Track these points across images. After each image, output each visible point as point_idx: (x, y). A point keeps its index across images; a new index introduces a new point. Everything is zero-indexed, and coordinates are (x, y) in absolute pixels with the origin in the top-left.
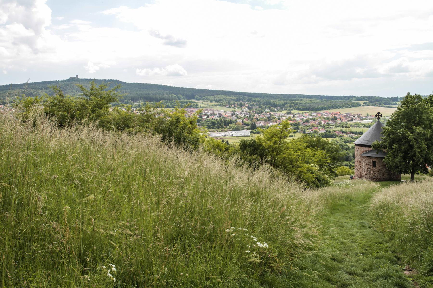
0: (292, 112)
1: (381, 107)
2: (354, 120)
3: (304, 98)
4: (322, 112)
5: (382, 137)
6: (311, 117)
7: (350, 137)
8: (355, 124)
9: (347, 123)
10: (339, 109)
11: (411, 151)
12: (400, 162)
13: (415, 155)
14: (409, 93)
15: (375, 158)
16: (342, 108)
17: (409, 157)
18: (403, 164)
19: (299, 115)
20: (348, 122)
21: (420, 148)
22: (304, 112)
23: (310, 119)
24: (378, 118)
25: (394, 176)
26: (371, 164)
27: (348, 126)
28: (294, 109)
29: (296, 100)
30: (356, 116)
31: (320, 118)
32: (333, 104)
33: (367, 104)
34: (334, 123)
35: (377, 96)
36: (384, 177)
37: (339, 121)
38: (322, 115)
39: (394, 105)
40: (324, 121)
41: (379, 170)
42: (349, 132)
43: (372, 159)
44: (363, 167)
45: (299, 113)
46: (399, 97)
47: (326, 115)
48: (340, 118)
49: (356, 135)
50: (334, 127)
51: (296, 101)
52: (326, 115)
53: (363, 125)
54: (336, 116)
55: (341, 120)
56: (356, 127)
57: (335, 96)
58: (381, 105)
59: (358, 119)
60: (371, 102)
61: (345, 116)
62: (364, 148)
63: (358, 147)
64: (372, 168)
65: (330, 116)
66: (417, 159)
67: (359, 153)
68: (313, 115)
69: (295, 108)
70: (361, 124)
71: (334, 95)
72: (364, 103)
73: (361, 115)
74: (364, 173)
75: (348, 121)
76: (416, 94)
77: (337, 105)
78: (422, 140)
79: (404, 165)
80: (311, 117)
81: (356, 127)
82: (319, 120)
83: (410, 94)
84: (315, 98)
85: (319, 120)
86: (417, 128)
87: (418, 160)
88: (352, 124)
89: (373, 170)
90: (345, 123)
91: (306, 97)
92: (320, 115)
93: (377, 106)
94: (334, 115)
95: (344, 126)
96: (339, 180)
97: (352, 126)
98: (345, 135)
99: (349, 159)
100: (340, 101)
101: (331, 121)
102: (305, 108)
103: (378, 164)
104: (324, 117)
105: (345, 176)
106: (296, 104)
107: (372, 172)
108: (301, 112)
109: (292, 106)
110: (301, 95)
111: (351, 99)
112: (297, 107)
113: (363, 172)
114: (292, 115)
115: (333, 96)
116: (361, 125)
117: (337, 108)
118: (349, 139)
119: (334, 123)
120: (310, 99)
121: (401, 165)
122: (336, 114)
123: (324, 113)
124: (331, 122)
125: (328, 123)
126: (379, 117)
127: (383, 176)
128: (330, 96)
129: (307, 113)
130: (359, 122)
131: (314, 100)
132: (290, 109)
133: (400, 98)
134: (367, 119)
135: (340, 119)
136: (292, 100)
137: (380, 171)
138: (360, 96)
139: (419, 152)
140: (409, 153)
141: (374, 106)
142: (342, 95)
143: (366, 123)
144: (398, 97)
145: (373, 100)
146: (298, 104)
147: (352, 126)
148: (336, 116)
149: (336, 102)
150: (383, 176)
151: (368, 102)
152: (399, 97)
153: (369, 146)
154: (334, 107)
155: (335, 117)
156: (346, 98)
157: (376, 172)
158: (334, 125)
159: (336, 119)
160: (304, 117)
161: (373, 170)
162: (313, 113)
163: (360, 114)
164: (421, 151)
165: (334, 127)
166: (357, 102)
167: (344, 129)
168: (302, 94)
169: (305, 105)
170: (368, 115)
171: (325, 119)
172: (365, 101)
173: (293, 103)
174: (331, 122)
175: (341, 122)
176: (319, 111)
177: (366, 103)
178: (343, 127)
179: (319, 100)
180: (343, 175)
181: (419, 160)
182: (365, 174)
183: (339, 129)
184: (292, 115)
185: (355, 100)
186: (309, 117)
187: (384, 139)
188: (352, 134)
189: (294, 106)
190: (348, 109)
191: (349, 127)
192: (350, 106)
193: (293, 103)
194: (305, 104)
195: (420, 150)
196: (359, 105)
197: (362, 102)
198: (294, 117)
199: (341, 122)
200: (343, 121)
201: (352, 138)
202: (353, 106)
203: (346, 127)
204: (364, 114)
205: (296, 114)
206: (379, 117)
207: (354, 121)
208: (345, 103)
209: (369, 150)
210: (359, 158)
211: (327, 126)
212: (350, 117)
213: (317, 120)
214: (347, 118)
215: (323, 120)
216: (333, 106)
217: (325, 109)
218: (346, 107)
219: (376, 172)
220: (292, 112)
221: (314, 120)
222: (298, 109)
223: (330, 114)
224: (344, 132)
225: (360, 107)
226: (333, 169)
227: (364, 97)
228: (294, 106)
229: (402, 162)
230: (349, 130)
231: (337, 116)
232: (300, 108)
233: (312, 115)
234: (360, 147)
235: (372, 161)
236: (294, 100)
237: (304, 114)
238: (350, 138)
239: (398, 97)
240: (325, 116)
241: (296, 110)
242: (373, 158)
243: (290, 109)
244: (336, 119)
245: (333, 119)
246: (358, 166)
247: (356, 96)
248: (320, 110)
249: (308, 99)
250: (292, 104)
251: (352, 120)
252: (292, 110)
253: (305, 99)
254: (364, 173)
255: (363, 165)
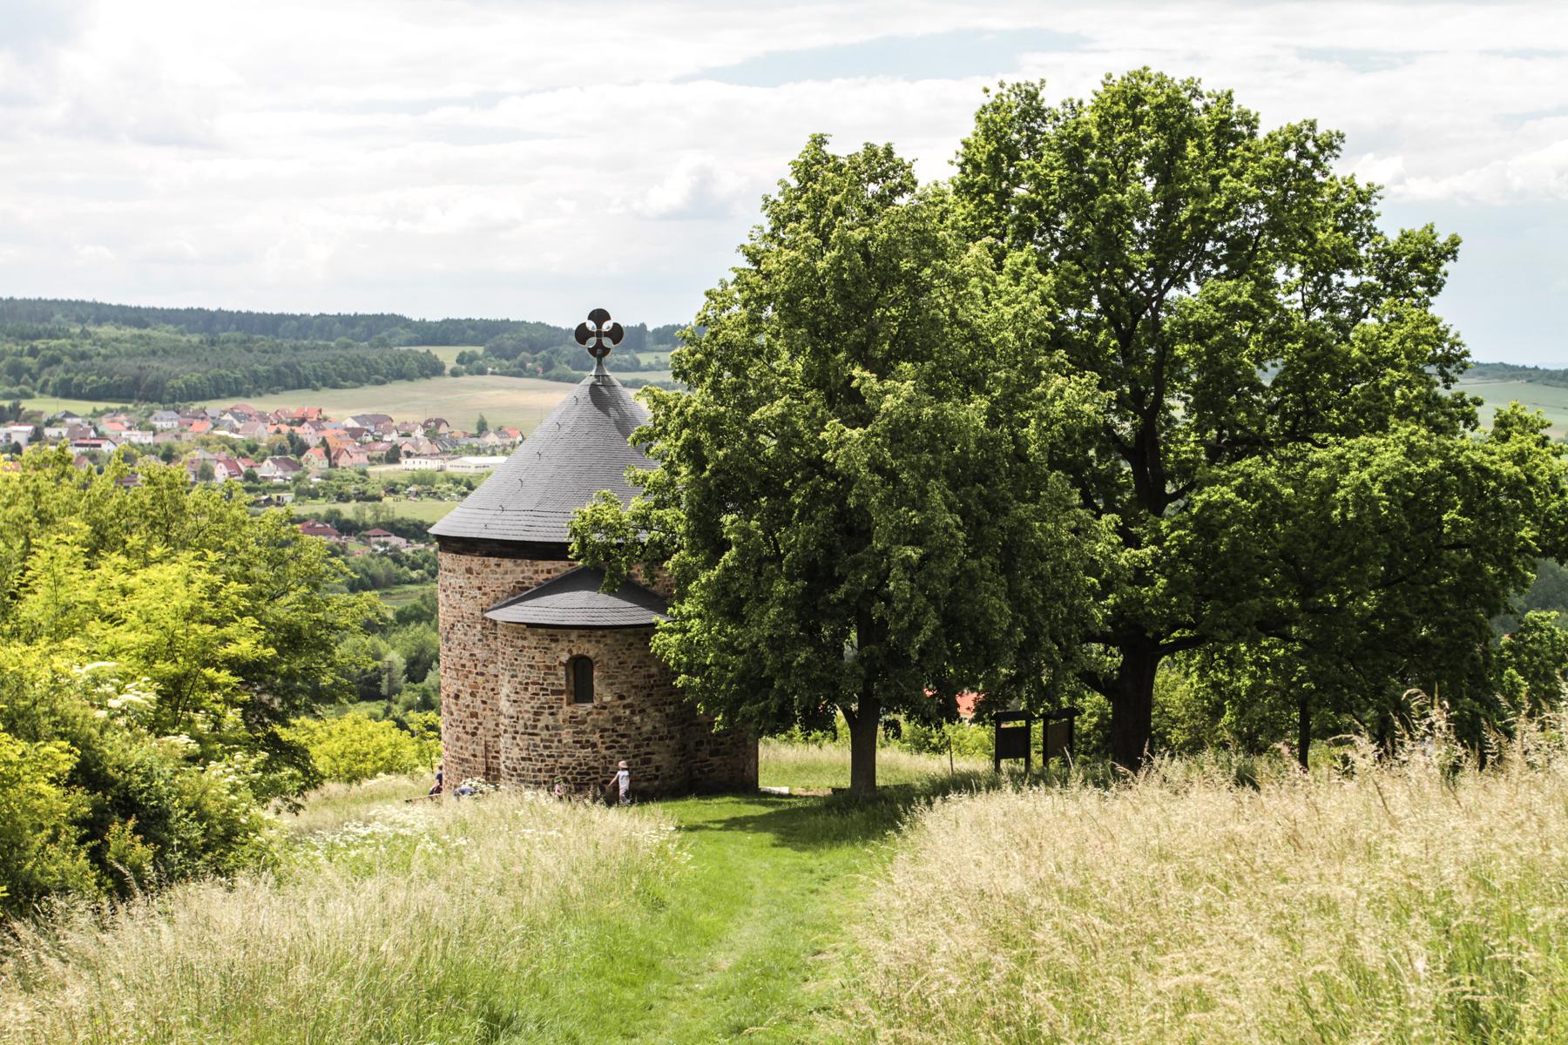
0: (28, 406)
1: (558, 379)
2: (409, 455)
3: (99, 322)
4: (213, 407)
5: (640, 472)
6: (148, 439)
7: (383, 554)
8: (414, 481)
9: (364, 473)
10: (315, 389)
11: (857, 565)
12: (777, 644)
13: (877, 591)
14: (819, 141)
15: (587, 630)
16: (335, 386)
17: (842, 602)
18: (802, 657)
19: (73, 430)
20: (370, 469)
21: (917, 536)
22: (101, 406)
23: (146, 450)
24: (593, 351)
25: (716, 760)
26: (561, 679)
27: (370, 492)
28: (42, 391)
29: (51, 336)
30: (419, 433)
31: (205, 444)
32: (280, 360)
33: (477, 363)
34: (291, 475)
35: (531, 320)
36: (651, 770)
37: (315, 462)
38: (215, 426)
39: (627, 370)
40: (229, 463)
41: (617, 720)
42: (378, 525)
43: (564, 644)
44: (504, 705)
45: (68, 415)
46: (650, 328)
47: (238, 425)
48: (324, 442)
49: (422, 546)
50: (288, 497)
51: (53, 343)
52: (238, 425)
53: (457, 482)
54: (298, 430)
55: (328, 453)
56: (417, 494)
57: (293, 317)
58: (553, 373)
59: (425, 446)
60: (500, 353)
61: (355, 434)
62: (507, 564)
63: (465, 560)
64: (567, 710)
65: (265, 434)
66: (900, 616)
67: (468, 607)
68: (158, 425)
69: (46, 383)
70: (449, 479)
71: (288, 311)
72: (460, 360)
73: (443, 429)
74: (510, 751)
75: (373, 460)
76: (869, 147)
77: (307, 368)
78: (930, 473)
79: (808, 664)
80: (148, 439)
81: (417, 494)
82: (198, 454)
83: (829, 150)
84: (170, 327)
85: (198, 454)
86: (888, 383)
87: (904, 623)
88: (396, 479)
89: (573, 720)
90: (352, 473)
91: (116, 320)
92: (201, 427)
93: (533, 374)
94: (285, 429)
95: (351, 489)
96: (329, 814)
97: (392, 489)
98: (353, 545)
99: (384, 690)
100: (320, 343)
101: (268, 461)
102: (107, 386)
103: (610, 678)
104: (225, 440)
105: (367, 783)
106: (55, 361)
107: (567, 736)
108: (84, 407)
109: (28, 370)
110: (82, 304)
111: (384, 334)
112: (57, 374)
113: (504, 742)
114: (30, 428)
115: (281, 318)
116: (444, 486)
117: (302, 383)
118: (379, 569)
119: (291, 475)
120: (136, 331)
121: (785, 669)
122: (302, 421)
123: (228, 417)
124: (268, 470)
125: (250, 476)
126: (599, 344)
127: (646, 762)
128: (264, 318)
129: (122, 417)
130: (431, 465)
131: (161, 334)
132: (15, 390)
133: (657, 331)
134: (478, 452)
135: (321, 450)
136: (24, 337)
137: (621, 729)
138: (434, 315)
139: (906, 563)
140: (841, 579)
141: (518, 375)
142: (332, 311)
143: (472, 471)
144: (643, 326)
145: (508, 341)
146: (66, 360)
147: (392, 489)
148: (298, 430)
149: (296, 349)
150: (646, 762)
151: (480, 350)
152: (650, 328)
153: (554, 551)
154: (290, 381)
155: (292, 438)
156: (358, 329)
157: (595, 738)
158: (285, 488)
159: (301, 448)
160: (101, 436)
161: (573, 720)
162: (158, 413)
163: (439, 422)
164: (923, 559)
165: (288, 497)
166: (422, 349)
167: (348, 510)
168: (89, 299)
169: (107, 365)
170: (482, 428)
171: (234, 448)
172: (468, 349)
173: (34, 352)
174: (268, 470)
175: (333, 465)
176: (197, 405)
177: (473, 358)
178: (343, 498)
179: (195, 339)
180: (353, 777)
181: (915, 627)
182: (516, 753)
183: (321, 507)
184: (30, 428)
185: (409, 343)
186: (135, 440)
187: (658, 488)
188: (395, 540)
189: (41, 369)
190: (369, 391)
191: (380, 499)
192: (377, 372)
193: (34, 352)
194: (106, 358)
195: (913, 553)
196: (436, 369)
197: (447, 355)
198: (37, 437)
199: (333, 465)
200: (343, 461)
201: (396, 559)
202: (400, 373)
203: (363, 497)
204: (459, 425)
205: (50, 423)
206: (599, 344)
207: (407, 464)
208: (352, 352)
209: (542, 577)
210: (470, 640)
211: (248, 490)
212: (378, 440)
213: (185, 458)
214: (363, 443)
215: (224, 454)
216: (277, 372)
217: (235, 390)
218: (359, 381)
219: (595, 738)
220: (28, 406)
221: (169, 456)
222: (67, 391)
223: (263, 418)
224: (348, 528)
225: (436, 381)
226: (287, 725)
227: (459, 322)
228: (41, 369)
229: (797, 642)
230: (377, 514)
231: (306, 433)
232: (79, 386)
233: (153, 429)
234: (475, 562)
235: (565, 657)
236: (37, 336)
237: (105, 426)
238: (388, 561)
239: (643, 326)
240: (237, 431)
241: (54, 395)
242: (574, 635)
243: (15, 390)
244: (301, 448)
245: (282, 450)
246: (466, 698)
247: (416, 318)
248: (203, 398)
249: (128, 332)
250: (28, 361)
251: (393, 456)
252: (29, 396)
253: (107, 331)
254: (510, 751)
255: (505, 690)
